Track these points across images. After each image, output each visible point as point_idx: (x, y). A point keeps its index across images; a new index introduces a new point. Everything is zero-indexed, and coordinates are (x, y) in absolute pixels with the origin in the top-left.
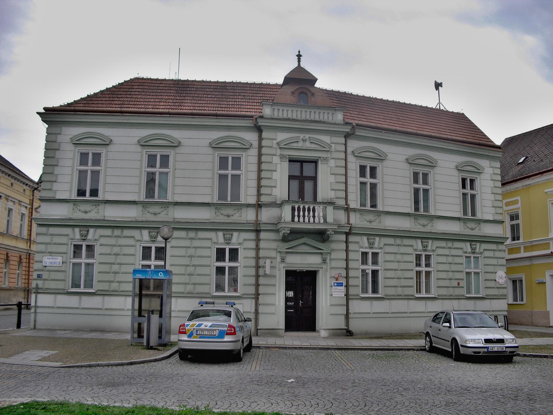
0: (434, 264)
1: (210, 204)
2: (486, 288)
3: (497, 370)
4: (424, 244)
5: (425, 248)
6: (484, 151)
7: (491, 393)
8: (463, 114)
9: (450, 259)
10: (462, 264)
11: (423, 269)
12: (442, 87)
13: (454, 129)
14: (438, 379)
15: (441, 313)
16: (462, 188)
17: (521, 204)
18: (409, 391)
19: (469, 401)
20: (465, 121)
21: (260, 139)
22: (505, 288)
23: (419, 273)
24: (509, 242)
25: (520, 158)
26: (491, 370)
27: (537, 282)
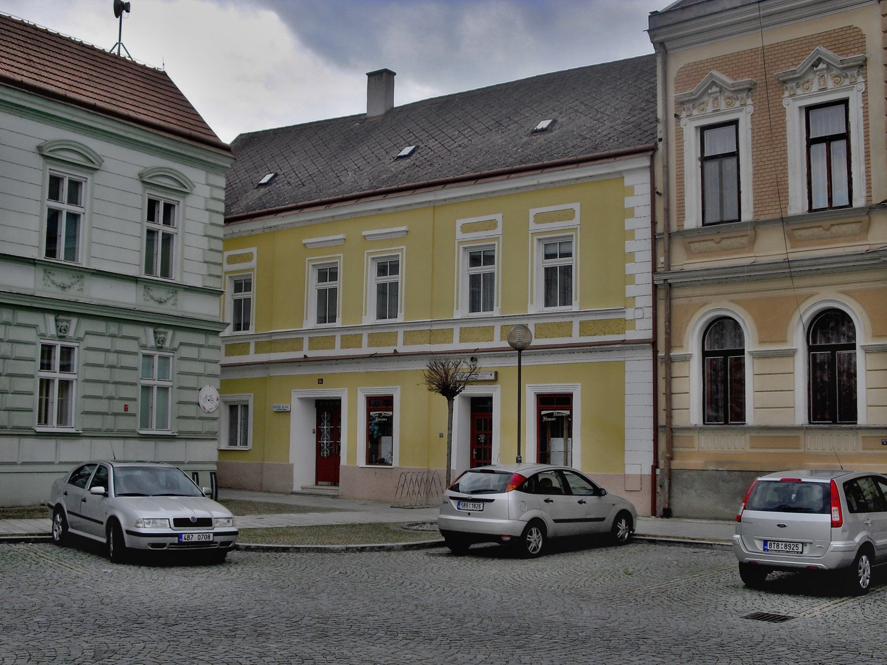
0: (173, 374)
1: (36, 262)
2: (179, 417)
3: (197, 579)
4: (60, 324)
6: (199, 151)
7: (185, 626)
8: (164, 74)
9: (112, 358)
10: (135, 369)
11: (56, 375)
12: (128, 11)
13: (144, 101)
14: (79, 602)
15: (89, 465)
16: (148, 220)
17: (258, 260)
18: (15, 632)
19: (142, 644)
20: (167, 88)
22: (215, 419)
23: (45, 384)
24: (228, 331)
25: (263, 175)
26: (186, 579)
27: (275, 410)
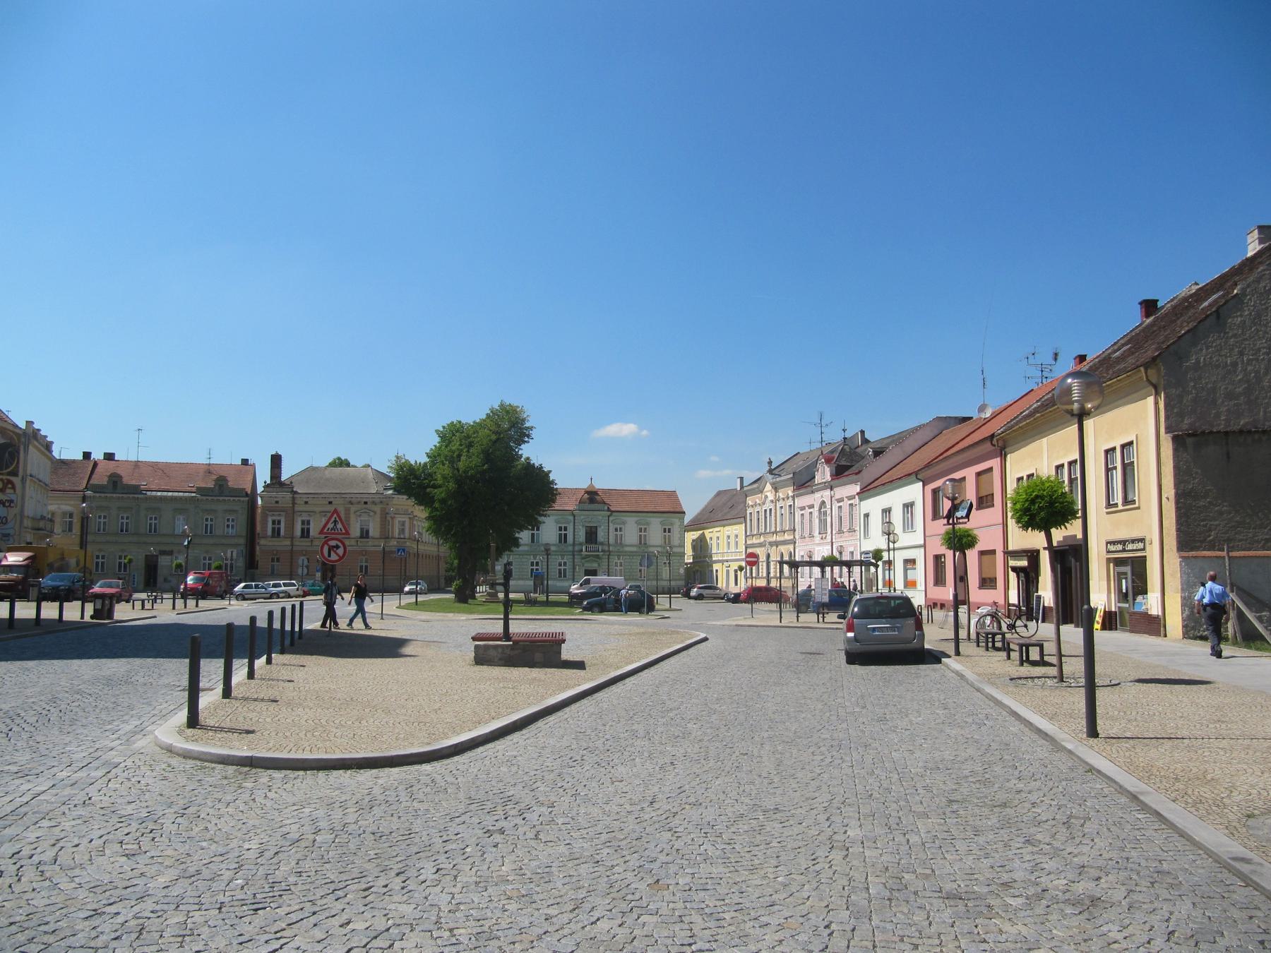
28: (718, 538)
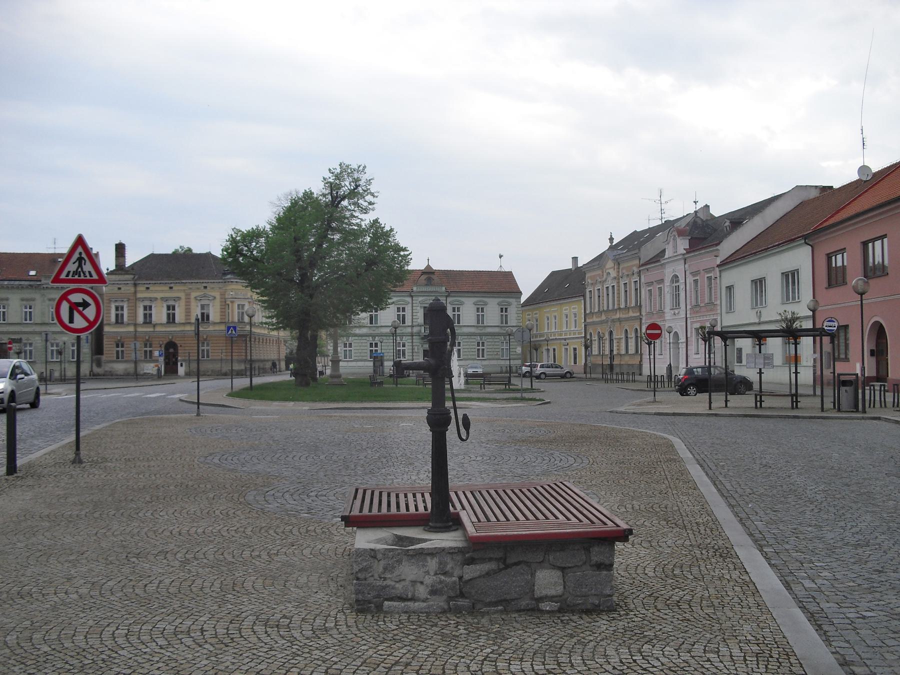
5: (481, 339)
9: (360, 344)
11: (481, 348)
21: (412, 300)
23: (478, 350)
28: (575, 314)
